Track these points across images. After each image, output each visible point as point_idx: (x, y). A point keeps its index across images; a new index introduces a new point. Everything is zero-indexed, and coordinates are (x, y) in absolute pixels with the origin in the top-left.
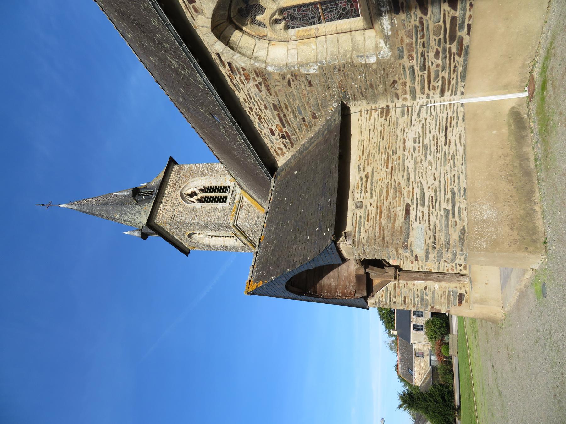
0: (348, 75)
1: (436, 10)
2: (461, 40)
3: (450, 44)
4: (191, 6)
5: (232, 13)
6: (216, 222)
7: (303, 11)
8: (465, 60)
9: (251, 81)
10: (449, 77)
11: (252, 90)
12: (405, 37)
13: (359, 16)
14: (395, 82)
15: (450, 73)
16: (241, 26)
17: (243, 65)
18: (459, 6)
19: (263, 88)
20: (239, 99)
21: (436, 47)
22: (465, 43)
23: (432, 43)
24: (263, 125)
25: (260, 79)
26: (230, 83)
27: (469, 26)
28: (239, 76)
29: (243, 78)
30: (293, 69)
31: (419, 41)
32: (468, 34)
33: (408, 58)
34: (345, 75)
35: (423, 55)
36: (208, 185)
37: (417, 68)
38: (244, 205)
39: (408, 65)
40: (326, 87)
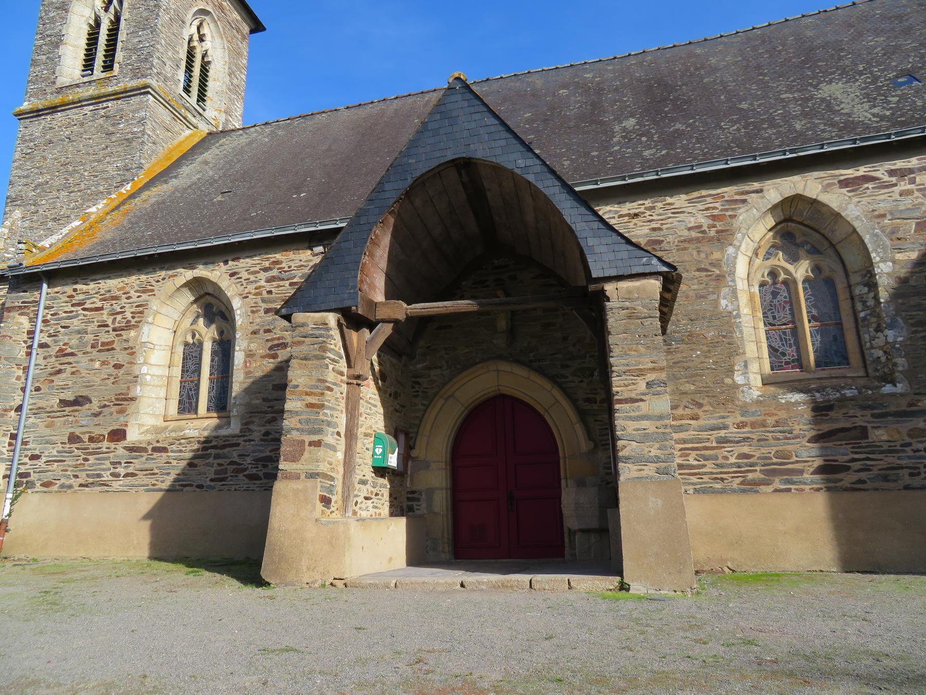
0: (715, 346)
1: (815, 452)
2: (767, 483)
3: (761, 471)
4: (836, 181)
5: (794, 225)
6: (157, 54)
7: (784, 307)
8: (734, 491)
9: (711, 222)
10: (705, 474)
11: (692, 219)
12: (776, 418)
13: (772, 369)
14: (700, 405)
15: (712, 473)
16: (775, 230)
17: (741, 218)
18: (817, 477)
19: (694, 234)
20: (671, 196)
21: (757, 454)
22: (763, 488)
23: (764, 450)
24: (614, 218)
25: (712, 233)
26: (704, 192)
27: (789, 490)
28: (720, 208)
29: (716, 212)
30: (729, 279)
31: (770, 435)
32: (776, 491)
33: (742, 422)
34: (714, 344)
35: (745, 439)
36: (211, 71)
37: (722, 433)
38: (178, 126)
39: (729, 421)
40: (693, 317)
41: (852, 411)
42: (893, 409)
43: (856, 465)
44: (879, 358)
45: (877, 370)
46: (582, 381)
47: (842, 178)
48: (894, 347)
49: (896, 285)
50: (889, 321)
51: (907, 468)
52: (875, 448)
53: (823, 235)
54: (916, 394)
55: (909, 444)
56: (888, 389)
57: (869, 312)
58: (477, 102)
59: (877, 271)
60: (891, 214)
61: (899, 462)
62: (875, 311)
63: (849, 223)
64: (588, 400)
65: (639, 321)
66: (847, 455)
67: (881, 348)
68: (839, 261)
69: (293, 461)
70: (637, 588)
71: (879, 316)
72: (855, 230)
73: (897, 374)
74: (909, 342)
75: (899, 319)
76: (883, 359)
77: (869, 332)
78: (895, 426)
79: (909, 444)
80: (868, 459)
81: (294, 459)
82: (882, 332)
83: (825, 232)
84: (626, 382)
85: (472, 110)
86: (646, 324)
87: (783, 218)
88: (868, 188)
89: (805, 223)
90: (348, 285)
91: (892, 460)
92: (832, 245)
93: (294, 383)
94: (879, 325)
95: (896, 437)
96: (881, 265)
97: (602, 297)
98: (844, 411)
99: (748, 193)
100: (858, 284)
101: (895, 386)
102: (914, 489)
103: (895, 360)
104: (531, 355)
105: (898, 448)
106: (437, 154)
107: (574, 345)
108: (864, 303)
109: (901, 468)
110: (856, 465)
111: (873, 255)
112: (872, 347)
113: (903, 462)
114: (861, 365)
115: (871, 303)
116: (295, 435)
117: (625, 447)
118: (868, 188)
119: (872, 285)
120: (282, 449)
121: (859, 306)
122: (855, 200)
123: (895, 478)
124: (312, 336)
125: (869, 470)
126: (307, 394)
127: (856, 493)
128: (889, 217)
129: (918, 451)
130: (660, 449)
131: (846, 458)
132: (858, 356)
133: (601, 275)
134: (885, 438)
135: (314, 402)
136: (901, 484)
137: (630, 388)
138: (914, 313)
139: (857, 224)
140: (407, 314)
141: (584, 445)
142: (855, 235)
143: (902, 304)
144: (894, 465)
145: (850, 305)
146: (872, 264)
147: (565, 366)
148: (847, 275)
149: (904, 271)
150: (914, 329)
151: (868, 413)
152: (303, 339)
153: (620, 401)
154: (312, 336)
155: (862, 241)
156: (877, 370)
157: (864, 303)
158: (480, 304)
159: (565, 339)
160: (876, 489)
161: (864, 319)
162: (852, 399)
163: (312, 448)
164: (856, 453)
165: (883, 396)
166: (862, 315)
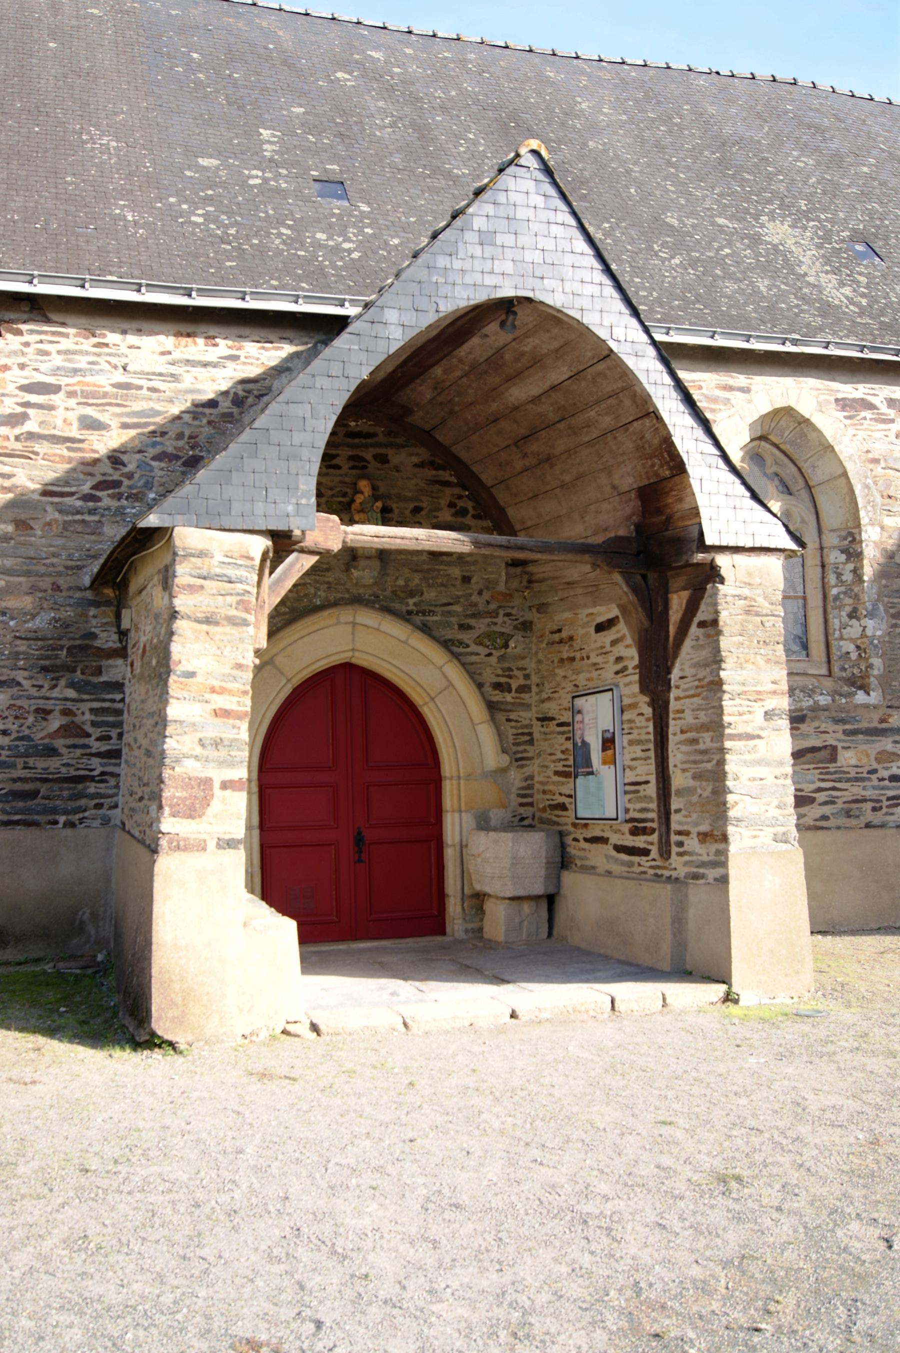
4: (832, 399)
5: (768, 446)
41: (824, 725)
42: (864, 725)
43: (821, 797)
44: (848, 653)
45: (843, 669)
46: (490, 655)
47: (840, 396)
48: (872, 643)
49: (881, 560)
50: (870, 607)
51: (871, 800)
52: (842, 777)
53: (799, 469)
54: (888, 707)
55: (875, 771)
56: (860, 697)
57: (843, 589)
58: (562, 206)
59: (864, 536)
60: (885, 460)
61: (864, 793)
62: (852, 590)
63: (841, 463)
64: (498, 686)
65: (758, 619)
66: (813, 782)
67: (852, 640)
68: (813, 510)
69: (191, 817)
70: (748, 997)
71: (856, 597)
72: (845, 474)
73: (872, 679)
74: (887, 639)
75: (880, 606)
76: (854, 656)
77: (840, 616)
78: (864, 747)
79: (875, 771)
80: (834, 789)
81: (192, 812)
82: (858, 619)
83: (805, 467)
84: (741, 709)
85: (551, 215)
86: (767, 624)
87: (759, 434)
88: (865, 418)
89: (781, 446)
90: (297, 489)
91: (856, 790)
92: (809, 487)
93: (185, 667)
94: (855, 610)
95: (865, 761)
96: (869, 528)
97: (713, 574)
98: (816, 724)
99: (730, 388)
100: (834, 547)
101: (869, 694)
102: (874, 827)
103: (871, 660)
104: (411, 601)
105: (865, 775)
106: (489, 280)
107: (480, 593)
108: (839, 575)
109: (866, 801)
110: (821, 797)
111: (862, 514)
112: (841, 638)
113: (868, 793)
114: (824, 659)
115: (848, 577)
116: (190, 768)
117: (736, 803)
118: (865, 418)
119: (853, 553)
120: (166, 794)
121: (832, 579)
122: (851, 431)
123: (857, 813)
124: (218, 577)
125: (833, 803)
126: (213, 690)
127: (819, 833)
128: (883, 464)
129: (883, 779)
130: (779, 807)
131: (813, 787)
132: (822, 647)
133: (717, 543)
134: (853, 762)
135: (228, 706)
136: (863, 821)
137: (745, 717)
138: (895, 600)
139: (850, 467)
140: (344, 542)
141: (491, 756)
142: (843, 480)
143: (886, 586)
144: (859, 798)
145: (820, 576)
146: (858, 526)
147: (463, 627)
148: (820, 532)
149: (891, 541)
150: (894, 621)
151: (840, 728)
152: (200, 582)
153: (733, 737)
154: (218, 577)
155: (852, 492)
156: (844, 669)
157: (839, 575)
158: (476, 543)
159: (466, 580)
160: (839, 828)
161: (836, 598)
162: (826, 709)
163: (228, 792)
164: (823, 780)
165: (857, 706)
166: (834, 591)
